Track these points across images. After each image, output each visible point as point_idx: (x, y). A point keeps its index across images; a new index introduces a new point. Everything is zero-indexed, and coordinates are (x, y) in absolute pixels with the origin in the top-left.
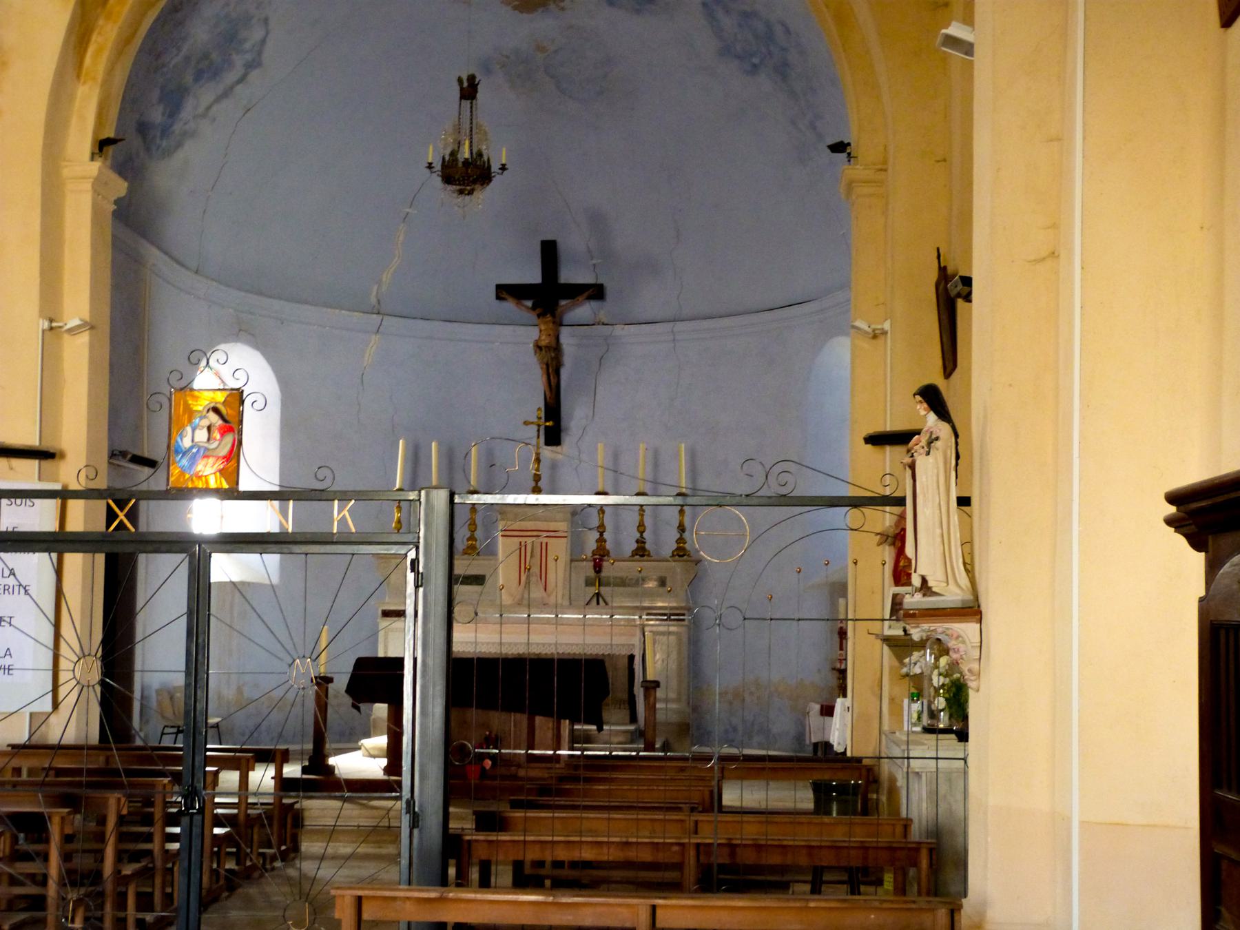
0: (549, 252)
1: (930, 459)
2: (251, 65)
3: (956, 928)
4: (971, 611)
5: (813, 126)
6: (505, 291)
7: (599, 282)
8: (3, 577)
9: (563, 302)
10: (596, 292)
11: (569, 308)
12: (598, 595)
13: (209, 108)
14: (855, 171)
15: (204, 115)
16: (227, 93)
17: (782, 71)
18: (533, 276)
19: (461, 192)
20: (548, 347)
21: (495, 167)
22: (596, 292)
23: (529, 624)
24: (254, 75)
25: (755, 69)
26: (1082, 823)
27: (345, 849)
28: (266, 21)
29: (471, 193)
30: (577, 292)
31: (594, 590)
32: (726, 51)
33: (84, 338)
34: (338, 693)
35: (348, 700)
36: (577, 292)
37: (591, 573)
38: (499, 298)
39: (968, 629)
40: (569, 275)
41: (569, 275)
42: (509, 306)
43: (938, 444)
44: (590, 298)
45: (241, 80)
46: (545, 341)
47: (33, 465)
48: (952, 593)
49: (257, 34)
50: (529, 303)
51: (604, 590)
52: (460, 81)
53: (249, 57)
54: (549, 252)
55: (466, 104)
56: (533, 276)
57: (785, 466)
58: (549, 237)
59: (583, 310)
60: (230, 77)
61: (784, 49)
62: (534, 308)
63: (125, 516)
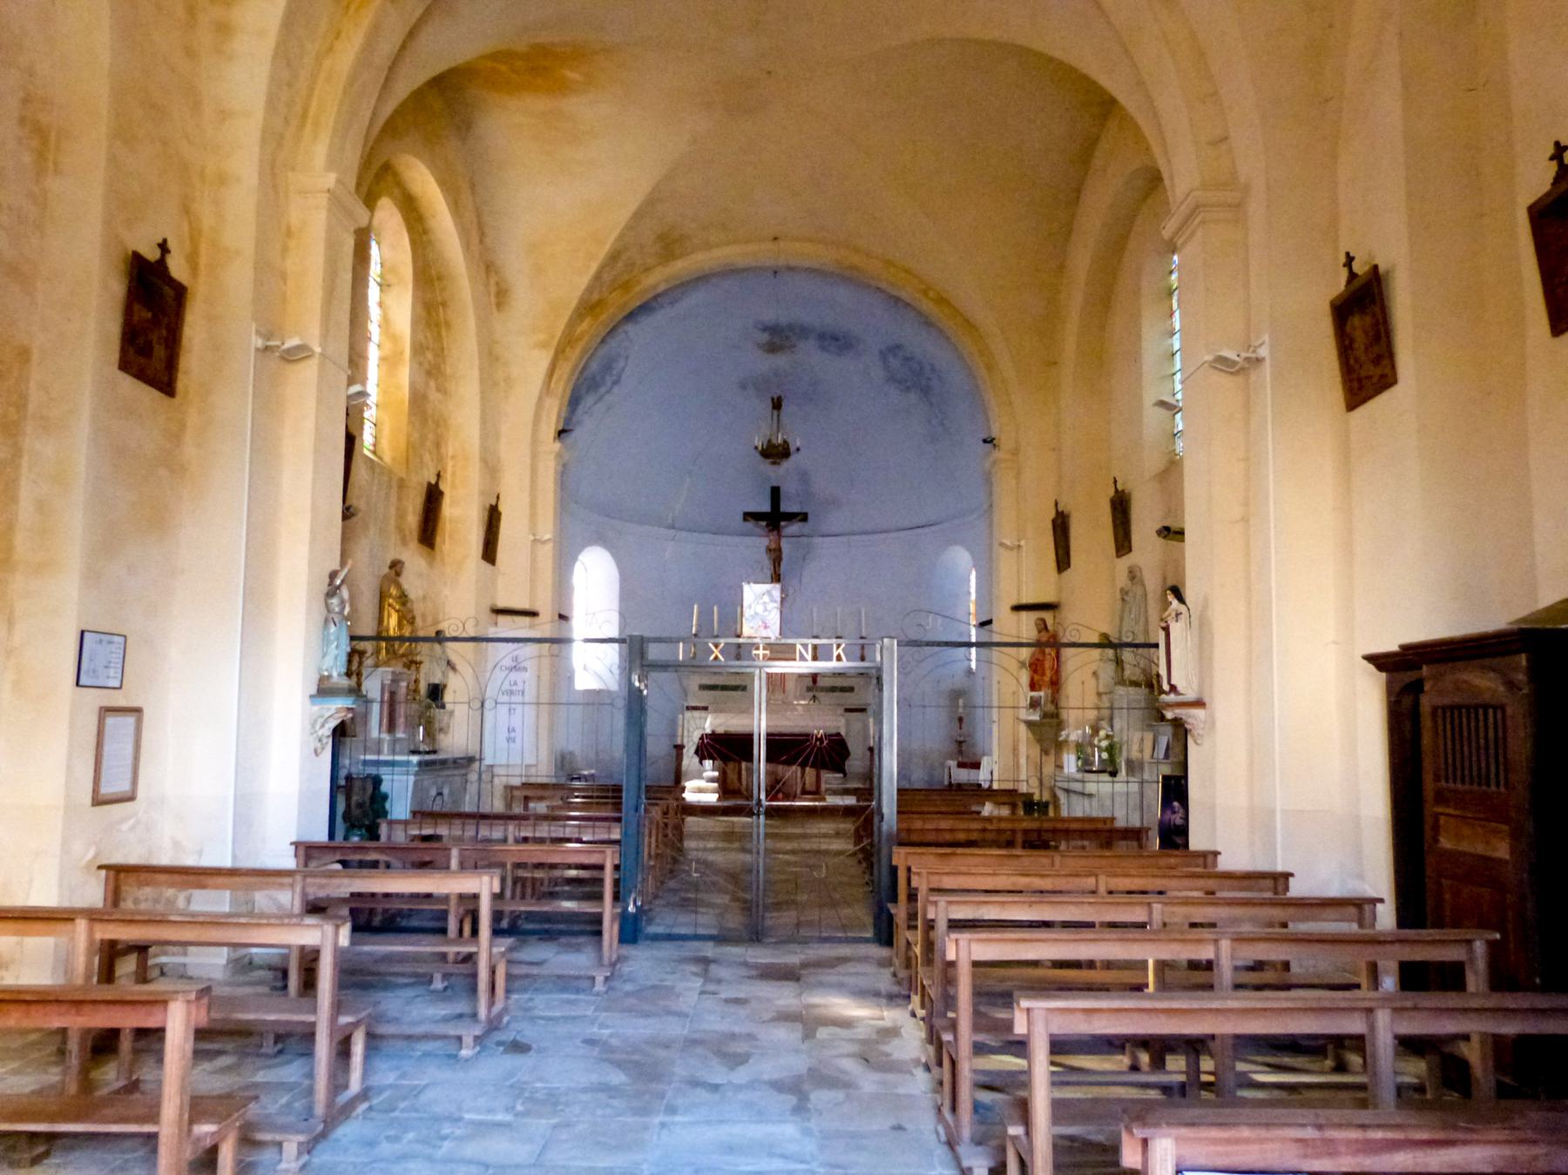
0: (775, 493)
1: (1178, 624)
2: (616, 382)
3: (5, 1007)
4: (1199, 703)
5: (942, 424)
6: (748, 516)
7: (804, 511)
8: (77, 684)
9: (783, 523)
10: (803, 517)
11: (785, 526)
12: (814, 697)
13: (590, 408)
14: (997, 454)
15: (586, 413)
16: (600, 399)
17: (926, 391)
18: (765, 507)
19: (774, 463)
20: (775, 550)
21: (792, 449)
22: (803, 517)
23: (1018, 708)
24: (616, 390)
25: (908, 389)
26: (1283, 811)
27: (711, 845)
28: (627, 357)
29: (779, 464)
30: (791, 517)
31: (811, 694)
32: (892, 379)
33: (549, 546)
34: (481, 760)
35: (696, 759)
36: (791, 517)
37: (811, 684)
38: (745, 520)
39: (1198, 713)
40: (785, 507)
41: (785, 507)
42: (750, 525)
43: (1182, 616)
44: (800, 520)
45: (609, 391)
46: (773, 546)
47: (526, 620)
48: (1190, 695)
49: (621, 364)
50: (764, 523)
51: (817, 694)
52: (773, 399)
53: (614, 378)
54: (775, 493)
55: (775, 412)
56: (765, 507)
57: (1076, 627)
58: (775, 484)
59: (793, 528)
60: (602, 390)
61: (929, 379)
62: (767, 526)
63: (713, 652)
